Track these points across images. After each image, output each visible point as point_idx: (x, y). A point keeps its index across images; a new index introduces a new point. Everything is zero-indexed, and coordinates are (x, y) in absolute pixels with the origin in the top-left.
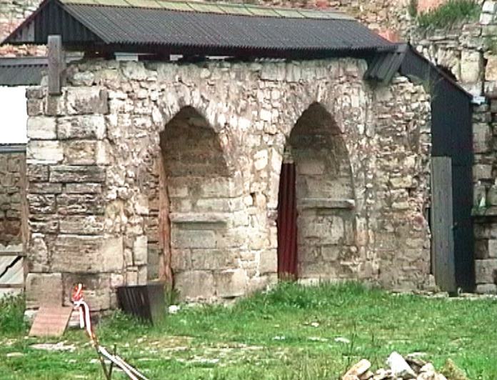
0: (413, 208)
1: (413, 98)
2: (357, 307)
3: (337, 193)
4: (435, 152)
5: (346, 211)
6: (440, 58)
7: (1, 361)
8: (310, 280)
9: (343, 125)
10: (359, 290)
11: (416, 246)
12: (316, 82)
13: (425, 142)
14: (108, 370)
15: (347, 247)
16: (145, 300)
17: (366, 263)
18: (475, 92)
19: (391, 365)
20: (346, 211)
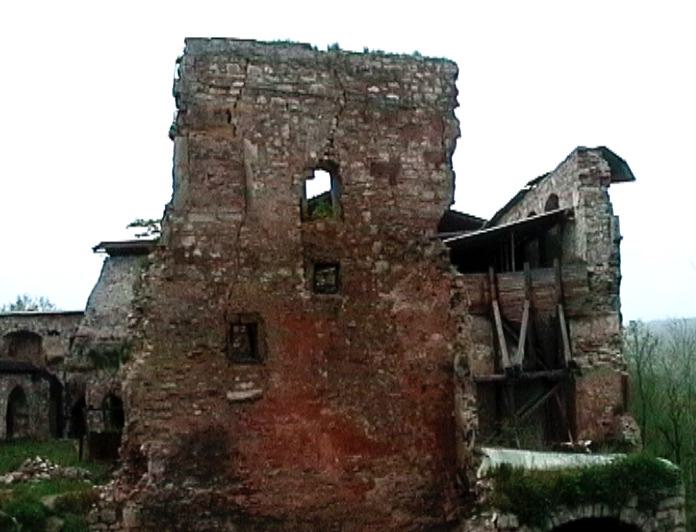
0: (45, 415)
1: (45, 384)
2: (461, 288)
3: (23, 411)
4: (51, 399)
5: (26, 416)
6: (53, 373)
7: (16, 441)
8: (16, 435)
9: (25, 392)
10: (29, 438)
11: (46, 426)
12: (18, 379)
13: (48, 396)
14: (640, 349)
15: (26, 426)
16: (593, 500)
17: (32, 429)
18: (63, 382)
19: (51, 302)
20: (26, 416)
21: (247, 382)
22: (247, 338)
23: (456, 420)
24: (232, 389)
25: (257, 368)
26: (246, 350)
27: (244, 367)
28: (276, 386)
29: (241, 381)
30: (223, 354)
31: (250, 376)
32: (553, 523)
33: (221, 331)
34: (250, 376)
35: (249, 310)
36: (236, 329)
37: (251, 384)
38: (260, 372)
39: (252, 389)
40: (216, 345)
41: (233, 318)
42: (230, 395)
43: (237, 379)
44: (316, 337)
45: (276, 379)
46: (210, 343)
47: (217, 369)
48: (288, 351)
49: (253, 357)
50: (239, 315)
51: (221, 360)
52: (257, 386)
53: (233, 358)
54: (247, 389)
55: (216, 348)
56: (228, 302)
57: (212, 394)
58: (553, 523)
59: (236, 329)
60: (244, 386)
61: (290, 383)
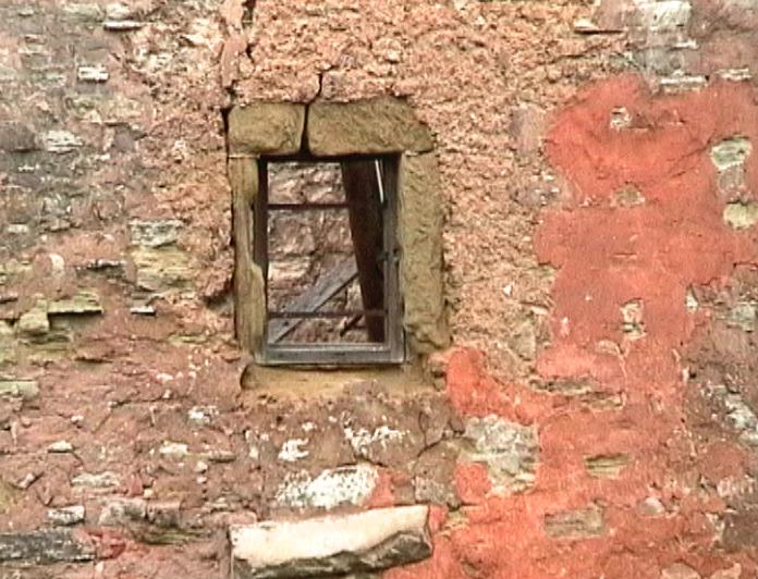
21: (348, 462)
22: (342, 234)
23: (387, 215)
24: (261, 508)
25: (398, 390)
26: (340, 297)
27: (332, 387)
28: (500, 489)
29: (310, 466)
30: (211, 318)
31: (359, 440)
32: (528, 538)
33: (210, 190)
34: (359, 440)
35: (356, 83)
36: (284, 185)
37: (363, 480)
38: (416, 414)
39: (370, 505)
40: (178, 267)
41: (265, 126)
42: (259, 543)
43: (290, 452)
44: (720, 228)
45: (498, 445)
46: (149, 264)
47: (183, 398)
48: (561, 297)
49: (377, 335)
50: (305, 104)
51: (199, 357)
52: (396, 490)
53: (270, 340)
54: (344, 508)
55: (179, 282)
56: (239, 39)
57: (155, 531)
58: (528, 538)
59: (284, 185)
60: (326, 488)
61: (574, 474)
